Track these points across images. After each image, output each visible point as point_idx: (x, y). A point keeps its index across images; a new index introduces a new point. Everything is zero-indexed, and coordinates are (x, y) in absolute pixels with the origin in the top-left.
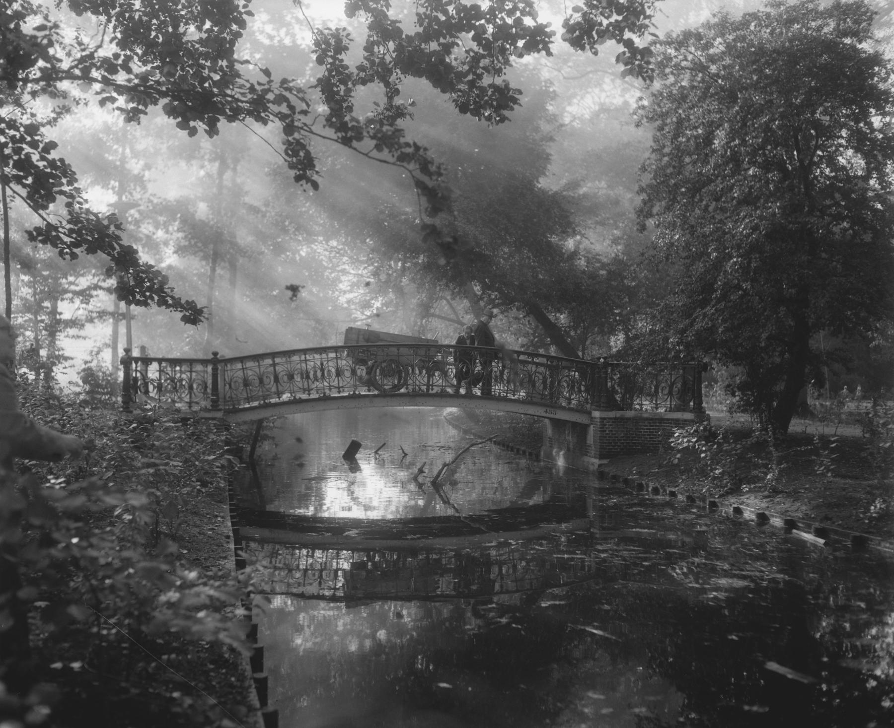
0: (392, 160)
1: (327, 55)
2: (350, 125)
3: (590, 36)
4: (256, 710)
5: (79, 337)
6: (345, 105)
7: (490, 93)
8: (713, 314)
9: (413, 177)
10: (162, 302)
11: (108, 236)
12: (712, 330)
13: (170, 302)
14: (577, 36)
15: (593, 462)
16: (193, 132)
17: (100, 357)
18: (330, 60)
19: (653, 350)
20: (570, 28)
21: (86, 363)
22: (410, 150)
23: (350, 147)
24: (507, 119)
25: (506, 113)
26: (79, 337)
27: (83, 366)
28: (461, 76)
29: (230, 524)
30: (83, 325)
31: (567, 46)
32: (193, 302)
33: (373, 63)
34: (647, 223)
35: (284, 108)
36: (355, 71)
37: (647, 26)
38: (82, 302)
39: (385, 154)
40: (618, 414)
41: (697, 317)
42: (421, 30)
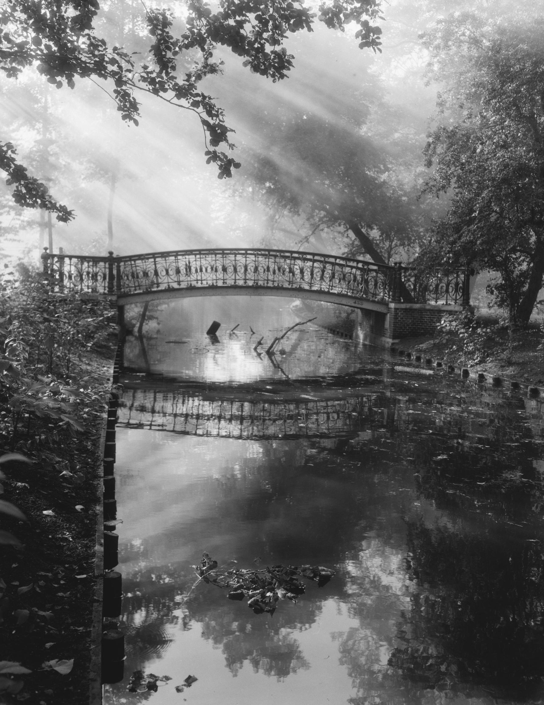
0: (188, 105)
1: (157, 29)
2: (157, 80)
3: (339, 19)
4: (101, 477)
5: (14, 240)
6: (170, 65)
7: (272, 57)
8: (475, 231)
9: (201, 117)
10: (44, 205)
11: (7, 158)
12: (472, 243)
13: (49, 205)
14: (329, 18)
15: (388, 341)
16: (59, 85)
17: (30, 255)
18: (160, 32)
19: (432, 258)
20: (325, 12)
21: (20, 259)
22: (199, 99)
23: (158, 95)
24: (286, 76)
25: (285, 72)
26: (14, 240)
27: (18, 262)
28: (251, 44)
29: (112, 372)
30: (18, 231)
31: (323, 25)
32: (64, 206)
33: (193, 33)
34: (433, 160)
35: (115, 68)
36: (181, 39)
37: (377, 12)
38: (16, 214)
39: (183, 102)
40: (408, 306)
41: (463, 233)
42: (222, 10)
